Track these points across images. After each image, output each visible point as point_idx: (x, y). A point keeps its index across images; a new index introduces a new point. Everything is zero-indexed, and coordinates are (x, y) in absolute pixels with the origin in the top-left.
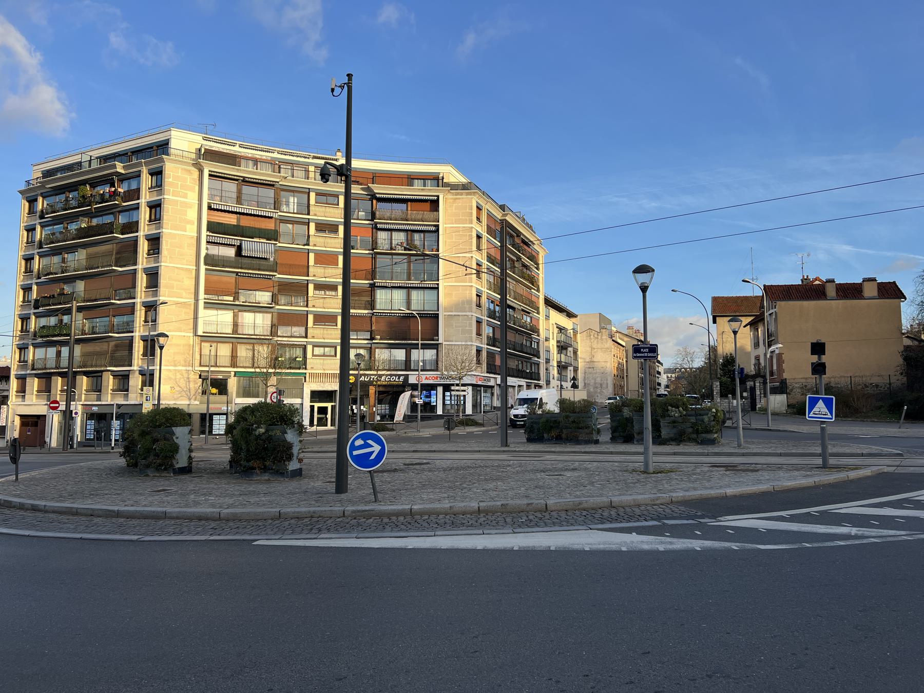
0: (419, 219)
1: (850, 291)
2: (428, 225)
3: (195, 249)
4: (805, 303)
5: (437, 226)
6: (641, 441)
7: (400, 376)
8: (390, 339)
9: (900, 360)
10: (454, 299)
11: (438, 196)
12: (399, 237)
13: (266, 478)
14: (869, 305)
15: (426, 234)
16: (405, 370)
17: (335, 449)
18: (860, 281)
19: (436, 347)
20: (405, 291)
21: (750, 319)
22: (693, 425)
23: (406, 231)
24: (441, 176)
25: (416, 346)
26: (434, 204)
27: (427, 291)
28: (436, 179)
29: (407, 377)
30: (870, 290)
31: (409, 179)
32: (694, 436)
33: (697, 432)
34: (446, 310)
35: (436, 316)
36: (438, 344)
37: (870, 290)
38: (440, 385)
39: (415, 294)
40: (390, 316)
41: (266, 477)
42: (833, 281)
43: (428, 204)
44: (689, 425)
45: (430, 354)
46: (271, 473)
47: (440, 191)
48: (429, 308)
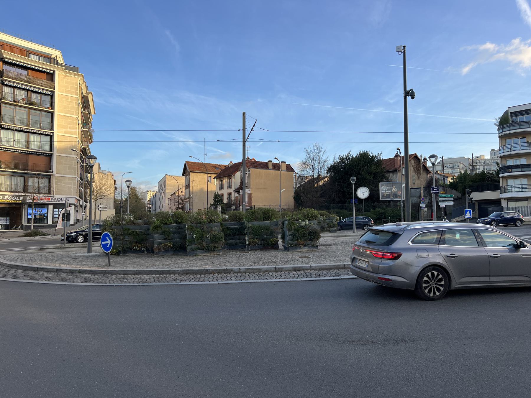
0: (38, 84)
1: (276, 167)
2: (46, 90)
3: (403, 113)
4: (256, 169)
5: (53, 92)
6: (352, 229)
7: (20, 196)
8: (14, 169)
9: (293, 200)
10: (63, 145)
11: (54, 71)
12: (20, 94)
13: (306, 250)
14: (283, 173)
15: (43, 96)
16: (24, 192)
17: (87, 246)
18: (267, 161)
19: (49, 178)
20: (24, 134)
21: (215, 176)
22: (328, 224)
23: (27, 90)
24: (53, 57)
25: (32, 175)
26: (51, 76)
27: (42, 136)
28: (48, 58)
29: (25, 197)
30: (283, 167)
31: (28, 52)
32: (328, 229)
33: (331, 227)
34: (60, 150)
35: (50, 156)
36: (50, 176)
37: (283, 167)
38: (51, 204)
39: (32, 137)
40: (14, 151)
41: (306, 249)
42: (285, 162)
43: (45, 75)
44: (326, 224)
45: (44, 182)
46: (309, 247)
47: (57, 68)
48: (45, 149)
